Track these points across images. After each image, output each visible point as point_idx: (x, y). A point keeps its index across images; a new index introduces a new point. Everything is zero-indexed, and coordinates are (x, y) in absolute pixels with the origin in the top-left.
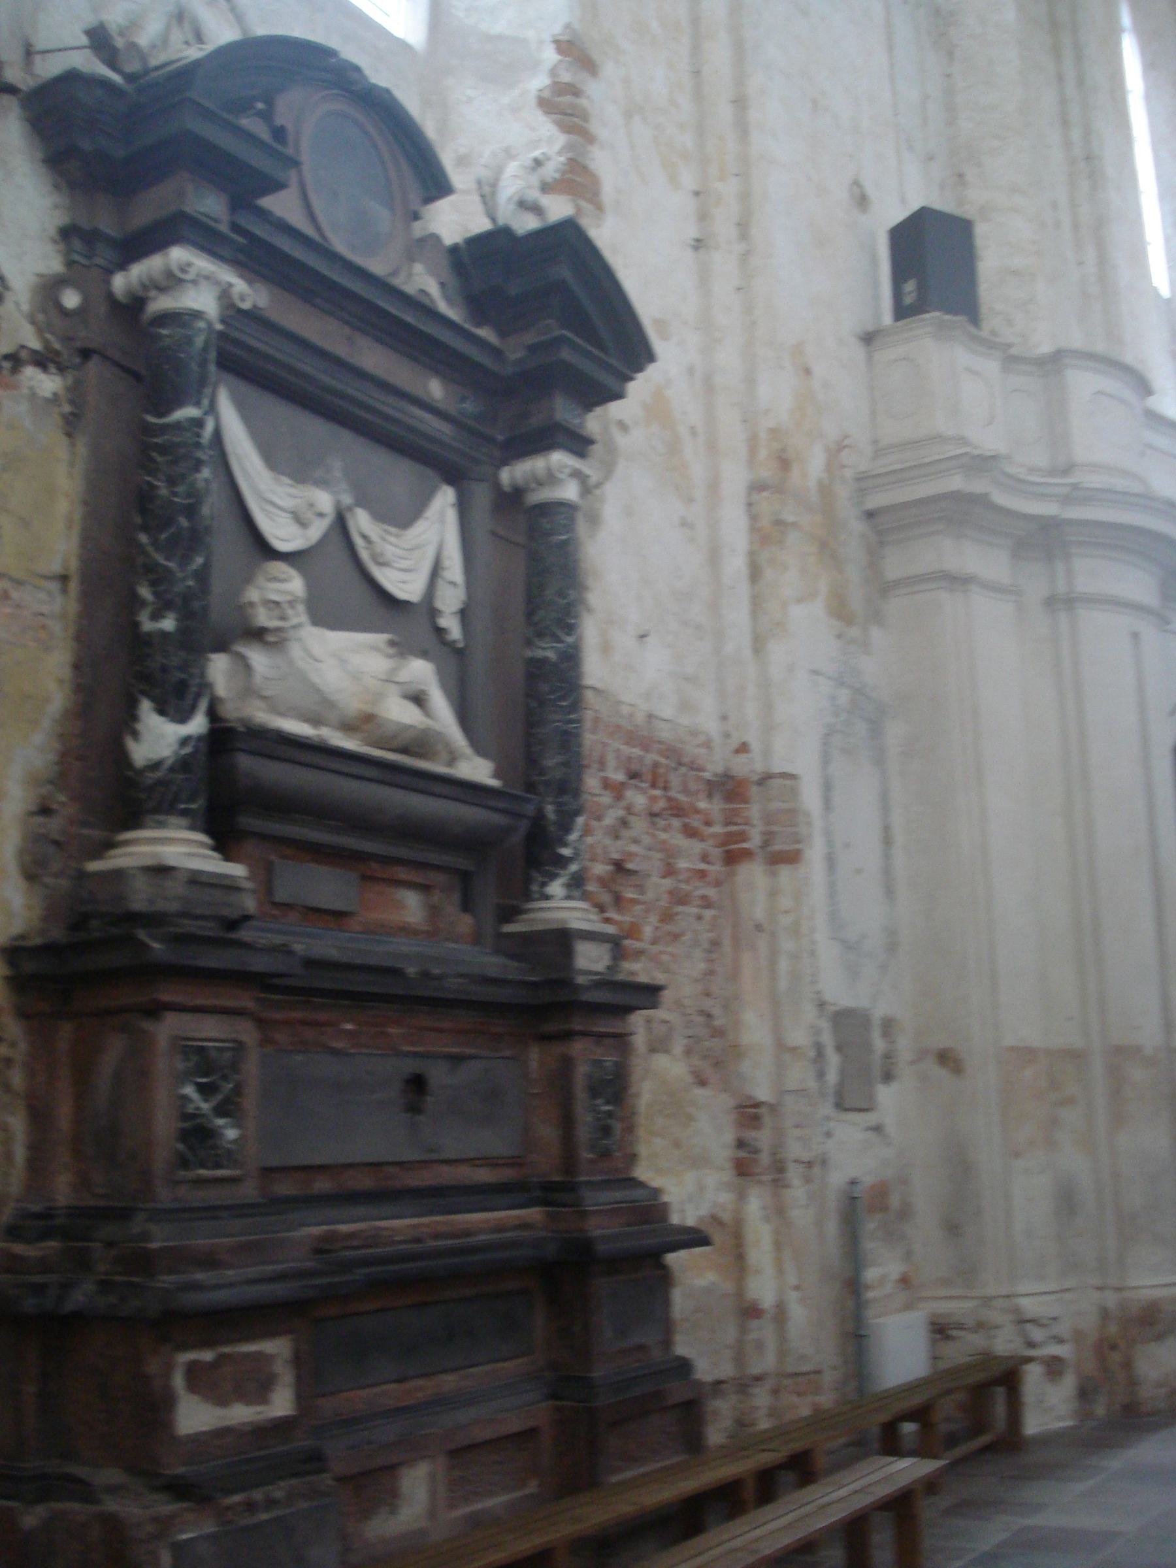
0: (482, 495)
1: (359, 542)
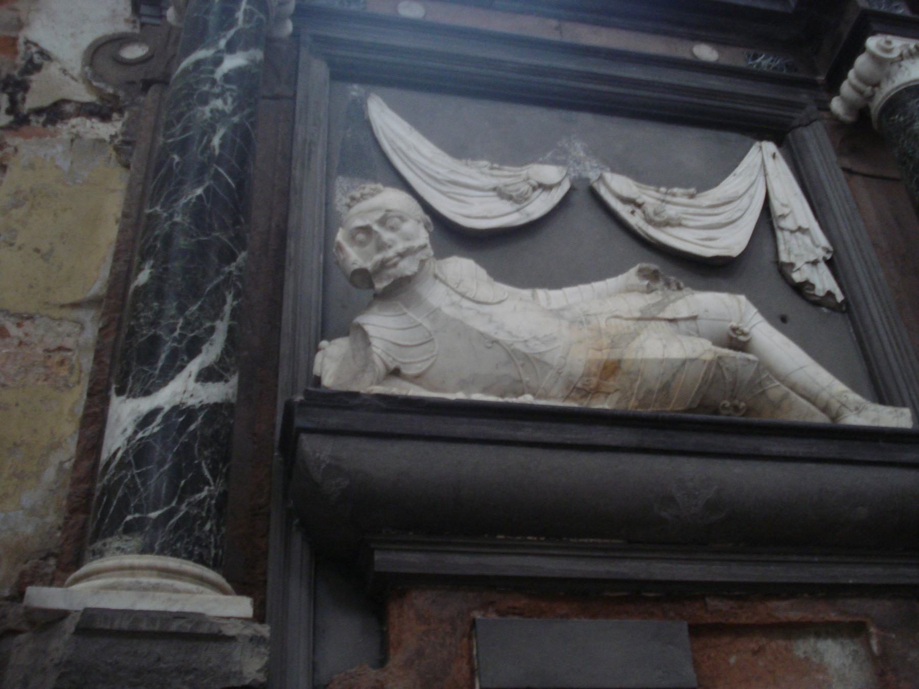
0: (816, 139)
1: (623, 211)
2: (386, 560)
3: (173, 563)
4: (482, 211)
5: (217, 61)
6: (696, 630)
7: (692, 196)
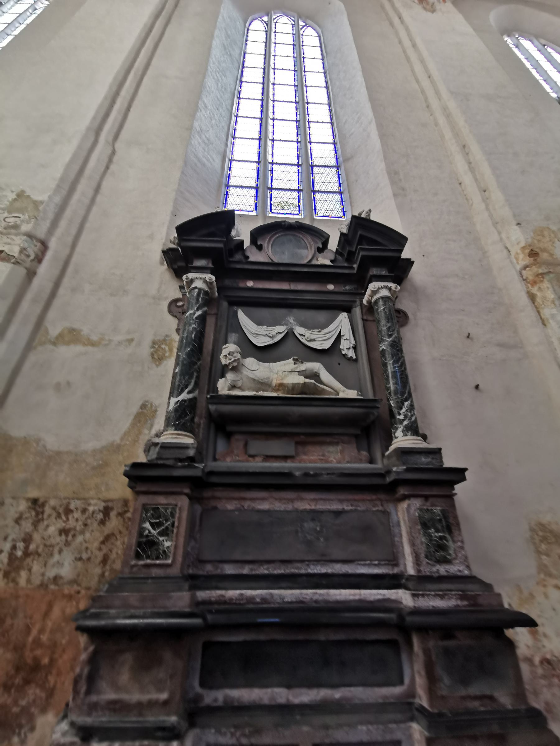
2: (230, 428)
3: (180, 432)
4: (260, 342)
5: (194, 314)
6: (297, 443)
7: (320, 332)
